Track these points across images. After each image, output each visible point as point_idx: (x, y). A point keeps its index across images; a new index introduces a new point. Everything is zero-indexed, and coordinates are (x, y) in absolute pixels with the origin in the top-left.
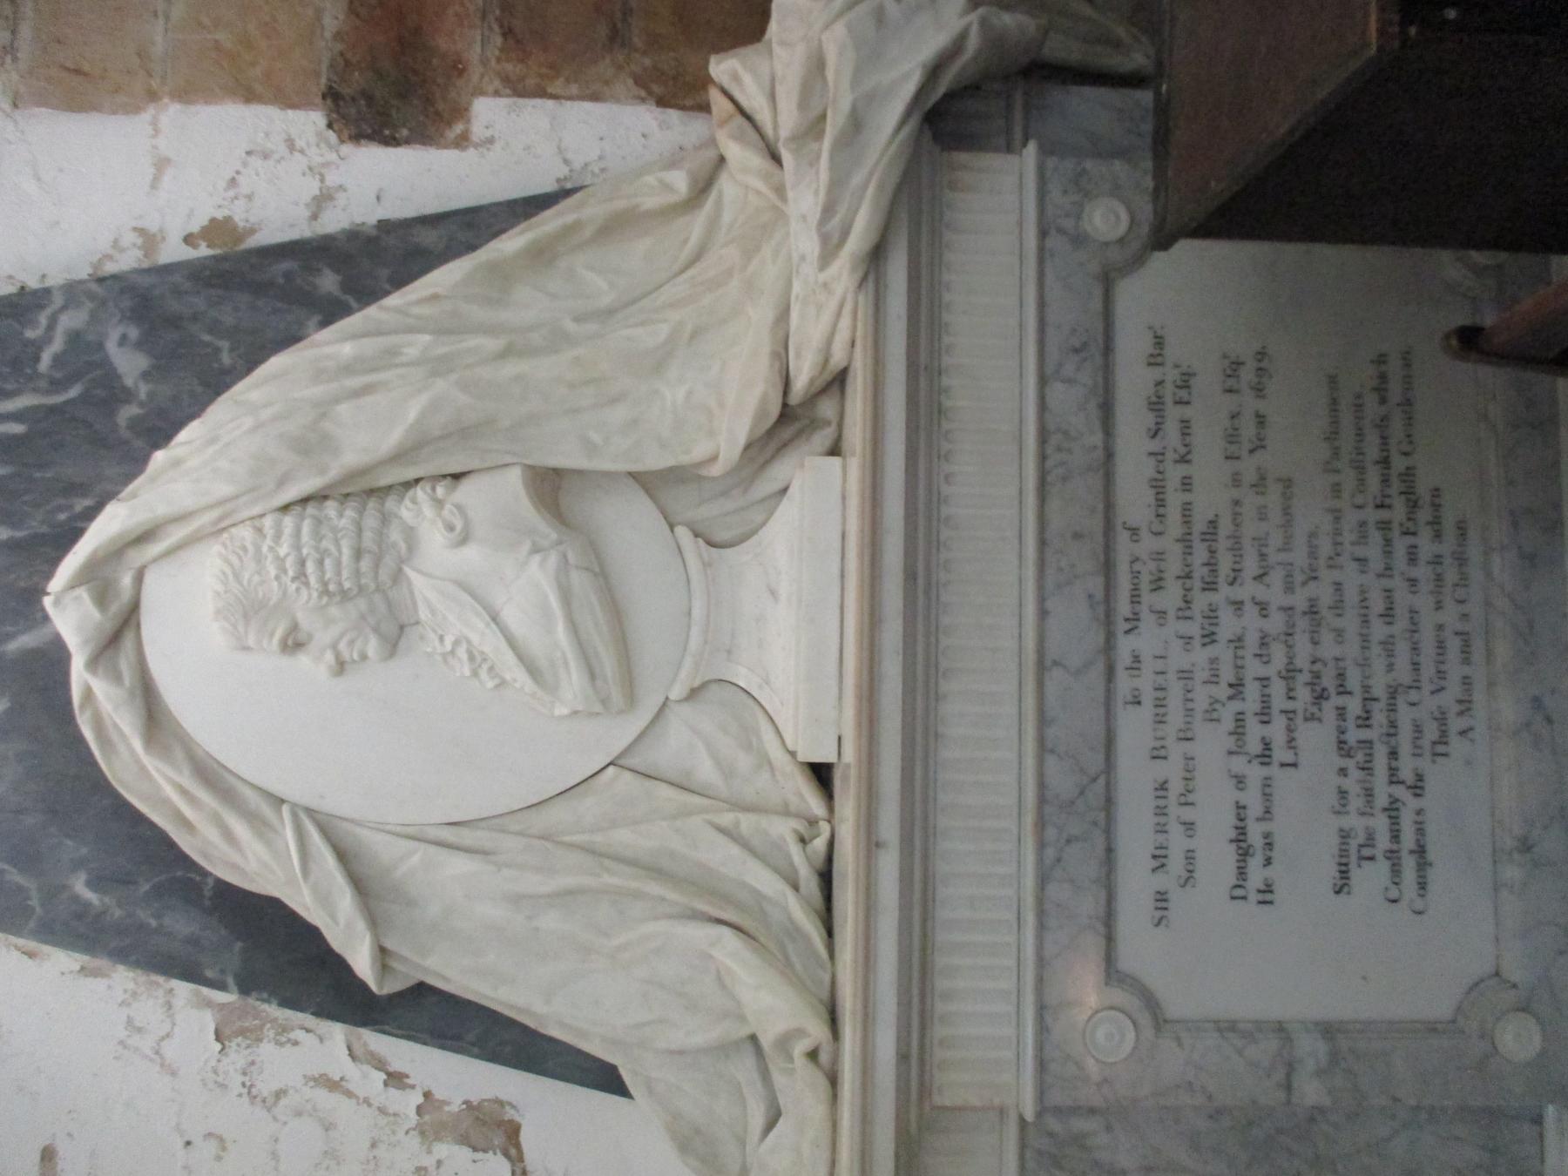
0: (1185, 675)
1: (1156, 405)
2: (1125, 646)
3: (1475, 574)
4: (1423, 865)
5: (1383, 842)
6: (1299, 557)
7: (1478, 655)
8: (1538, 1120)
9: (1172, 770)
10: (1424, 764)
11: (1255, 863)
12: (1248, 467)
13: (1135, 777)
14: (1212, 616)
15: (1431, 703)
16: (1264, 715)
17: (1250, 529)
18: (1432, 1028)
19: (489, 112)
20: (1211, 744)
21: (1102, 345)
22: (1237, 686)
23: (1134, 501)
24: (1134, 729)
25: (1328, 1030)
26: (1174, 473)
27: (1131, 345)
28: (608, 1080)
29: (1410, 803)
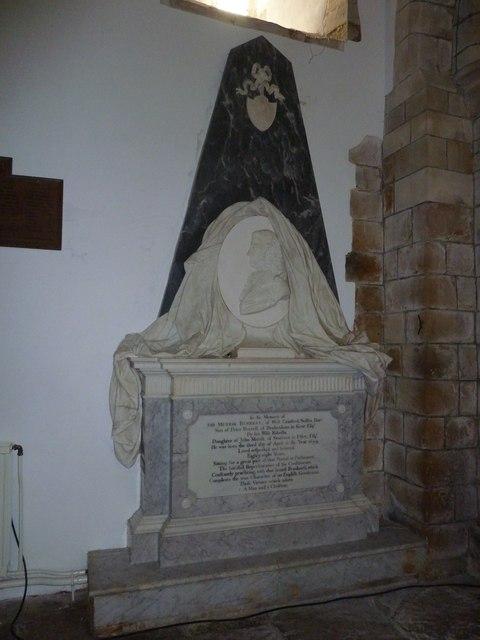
0: (256, 428)
1: (307, 420)
2: (261, 415)
3: (276, 489)
4: (219, 481)
5: (224, 472)
6: (279, 452)
7: (261, 491)
8: (162, 514)
9: (238, 426)
10: (240, 480)
11: (220, 445)
12: (296, 440)
13: (236, 418)
14: (268, 434)
15: (251, 481)
16: (249, 445)
17: (285, 441)
18: (187, 485)
19: (352, 286)
20: (243, 434)
21: (319, 407)
22: (254, 439)
23: (290, 416)
24: (246, 418)
25: (187, 462)
26: (294, 424)
27: (318, 415)
28: (165, 308)
29: (231, 478)
